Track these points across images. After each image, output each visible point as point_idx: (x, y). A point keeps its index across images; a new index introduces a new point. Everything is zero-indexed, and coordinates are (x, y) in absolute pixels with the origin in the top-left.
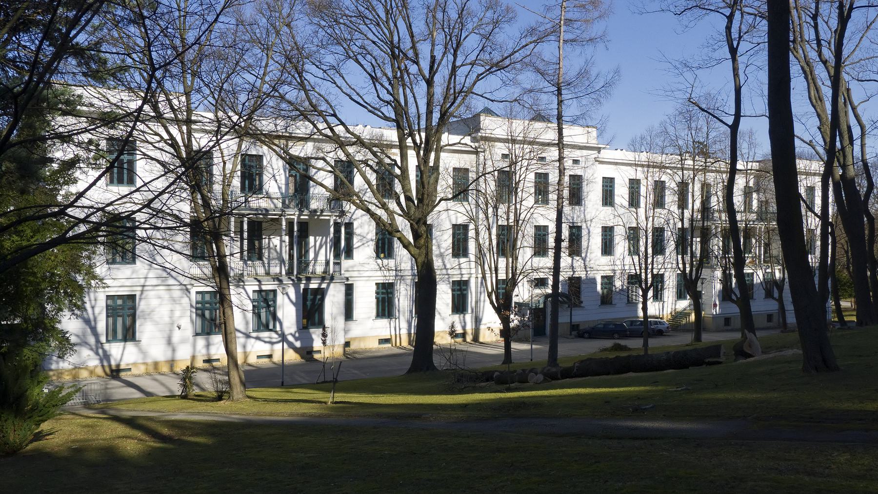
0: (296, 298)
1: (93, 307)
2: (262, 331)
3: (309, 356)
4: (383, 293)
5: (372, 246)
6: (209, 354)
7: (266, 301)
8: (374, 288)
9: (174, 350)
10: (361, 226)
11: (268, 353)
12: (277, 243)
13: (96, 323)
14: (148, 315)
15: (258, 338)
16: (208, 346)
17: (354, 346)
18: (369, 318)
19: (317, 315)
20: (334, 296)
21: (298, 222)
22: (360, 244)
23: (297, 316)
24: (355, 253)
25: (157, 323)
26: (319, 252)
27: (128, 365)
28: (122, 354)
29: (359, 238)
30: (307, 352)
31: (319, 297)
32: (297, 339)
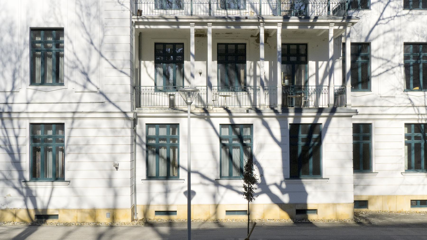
0: (282, 136)
1: (17, 137)
2: (236, 178)
3: (299, 216)
4: (417, 138)
5: (401, 72)
6: (167, 206)
7: (241, 138)
8: (404, 131)
9: (116, 195)
10: (385, 45)
11: (246, 208)
12: (262, 68)
13: (20, 157)
14: (82, 149)
15: (229, 187)
16: (167, 192)
17: (372, 208)
18: (397, 170)
19: (311, 161)
20: (337, 134)
21: (283, 35)
22: (381, 70)
23: (284, 160)
24: (374, 82)
25: (93, 161)
26: (323, 77)
27: (58, 210)
28: (51, 197)
29: (381, 62)
30: (299, 212)
31: (315, 136)
32: (283, 192)
